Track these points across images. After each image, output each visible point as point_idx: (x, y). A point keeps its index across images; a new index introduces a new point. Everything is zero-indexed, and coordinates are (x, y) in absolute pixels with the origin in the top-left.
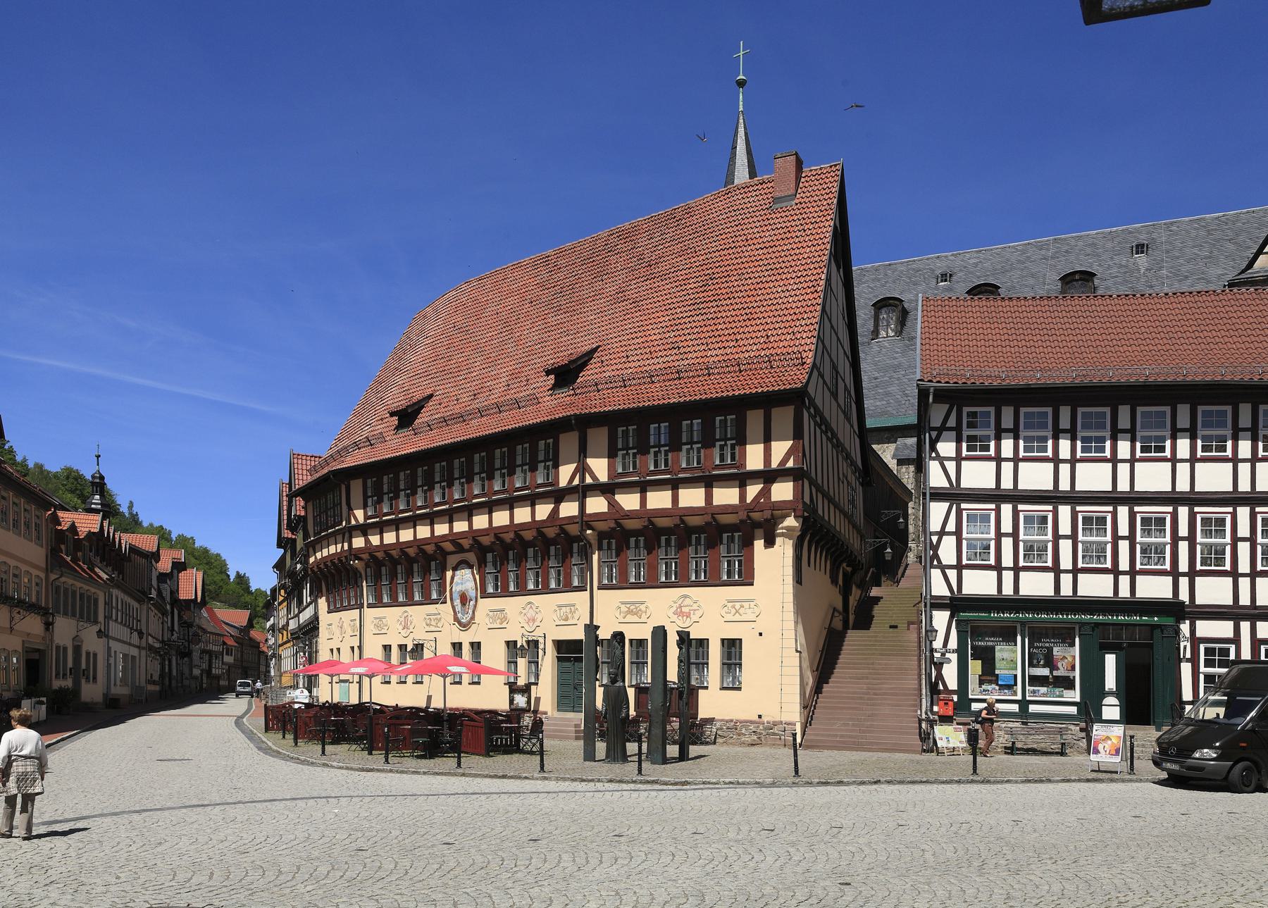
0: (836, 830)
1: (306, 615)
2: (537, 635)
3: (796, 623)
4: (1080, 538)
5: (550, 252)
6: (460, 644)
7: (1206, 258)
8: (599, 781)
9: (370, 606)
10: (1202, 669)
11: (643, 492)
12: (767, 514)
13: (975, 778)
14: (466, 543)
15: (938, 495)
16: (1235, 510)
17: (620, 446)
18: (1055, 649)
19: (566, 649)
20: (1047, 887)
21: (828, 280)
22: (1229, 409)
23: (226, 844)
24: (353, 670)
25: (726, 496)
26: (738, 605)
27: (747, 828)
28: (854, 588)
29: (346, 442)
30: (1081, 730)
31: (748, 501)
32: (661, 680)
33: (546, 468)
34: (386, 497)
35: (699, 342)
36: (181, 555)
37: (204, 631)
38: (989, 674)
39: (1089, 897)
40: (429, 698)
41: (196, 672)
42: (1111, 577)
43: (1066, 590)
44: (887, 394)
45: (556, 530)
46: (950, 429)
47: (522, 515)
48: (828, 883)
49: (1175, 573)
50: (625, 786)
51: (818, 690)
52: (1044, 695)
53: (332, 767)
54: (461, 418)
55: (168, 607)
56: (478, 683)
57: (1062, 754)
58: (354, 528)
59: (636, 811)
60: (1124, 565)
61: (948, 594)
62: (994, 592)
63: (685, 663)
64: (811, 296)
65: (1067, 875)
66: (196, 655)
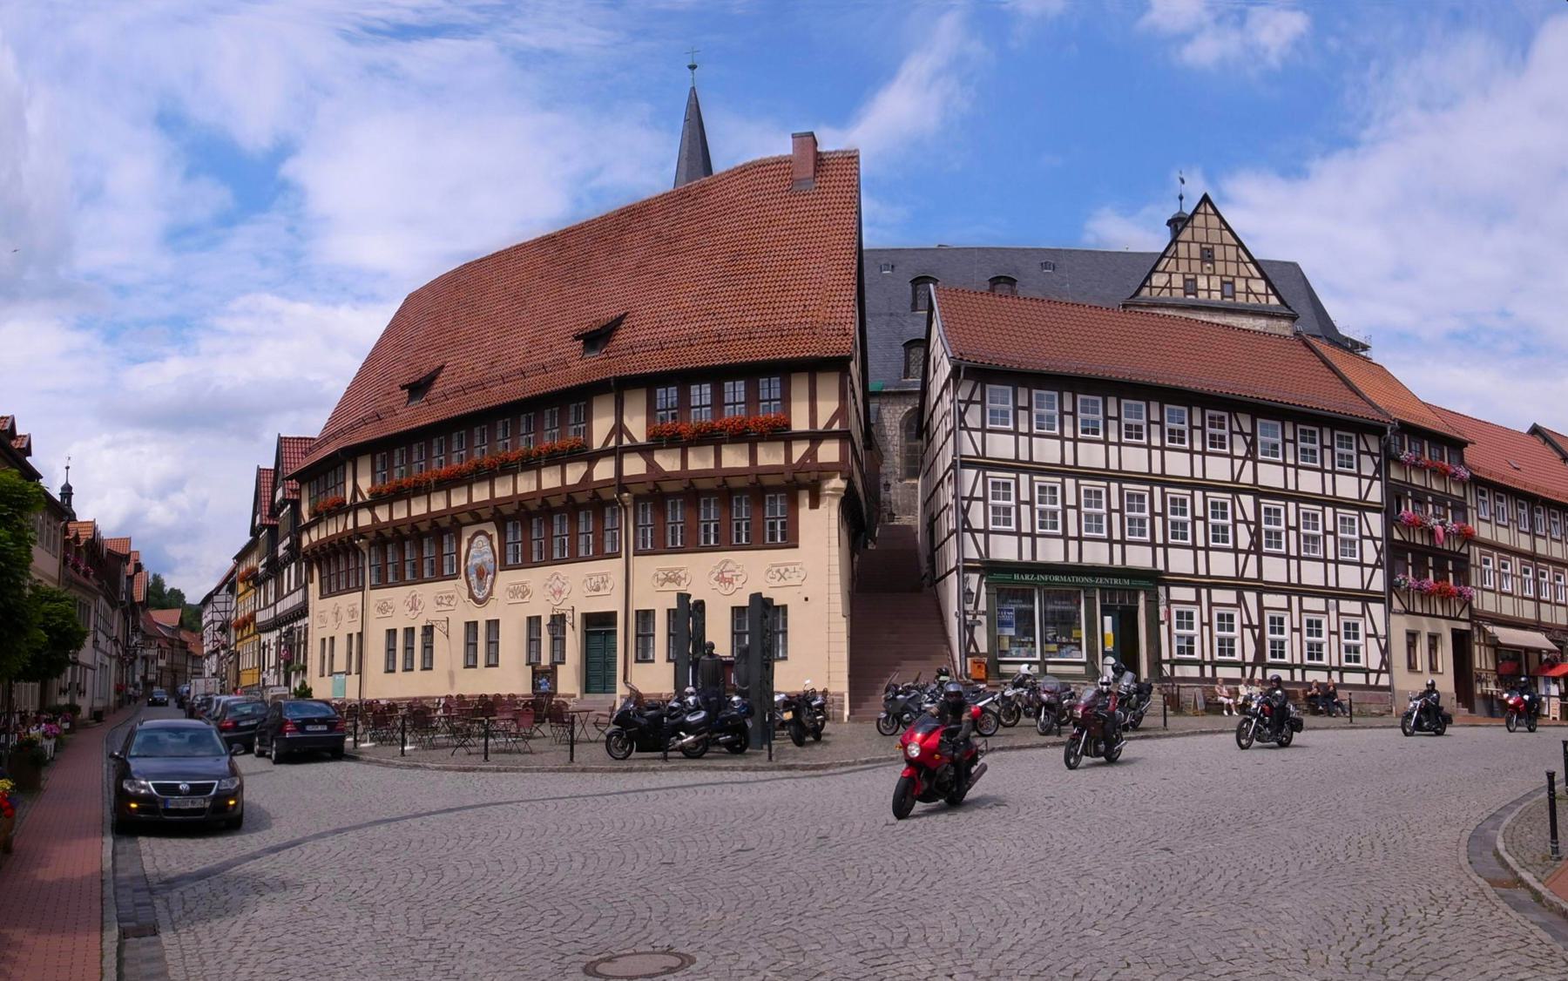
2: (564, 608)
9: (373, 587)
12: (814, 476)
45: (590, 494)
54: (481, 385)
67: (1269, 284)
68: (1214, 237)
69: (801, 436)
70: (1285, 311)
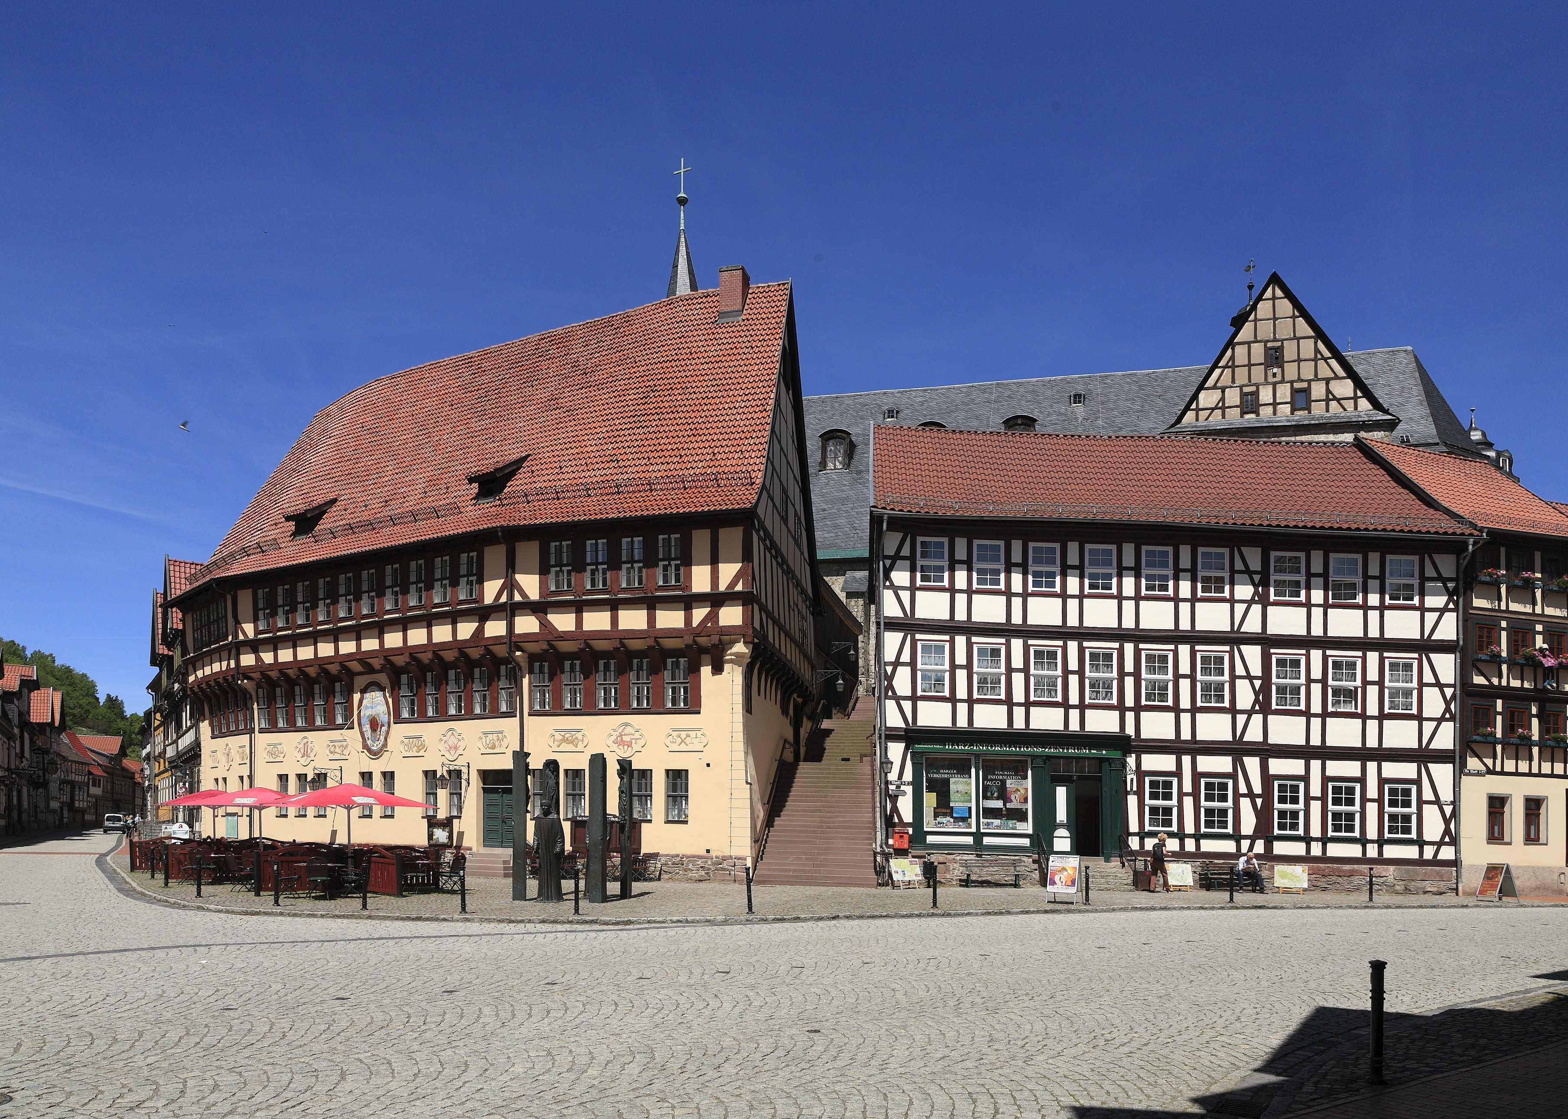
0: (797, 971)
1: (186, 741)
2: (460, 764)
3: (746, 753)
4: (1032, 671)
5: (471, 354)
6: (370, 774)
7: (1138, 411)
8: (530, 921)
9: (261, 731)
10: (1148, 801)
11: (579, 612)
12: (715, 639)
13: (935, 911)
14: (376, 663)
15: (892, 625)
16: (1176, 648)
17: (553, 562)
18: (1008, 782)
19: (492, 780)
20: (1029, 1027)
21: (777, 400)
22: (1170, 549)
23: (49, 1005)
24: (238, 801)
25: (670, 619)
26: (683, 735)
27: (700, 970)
28: (805, 720)
29: (233, 548)
30: (1034, 862)
31: (695, 624)
32: (600, 812)
33: (470, 583)
34: (280, 610)
35: (639, 455)
36: (33, 673)
37: (65, 759)
38: (944, 807)
39: (1074, 1035)
40: (334, 833)
41: (55, 805)
42: (1062, 710)
43: (1019, 723)
44: (836, 526)
45: (481, 651)
46: (904, 558)
47: (442, 633)
48: (794, 1031)
49: (1121, 708)
50: (559, 927)
51: (769, 823)
52: (998, 827)
53: (209, 910)
54: (370, 526)
55: (16, 731)
56: (392, 817)
57: (1016, 885)
58: (234, 642)
59: (573, 955)
60: (1074, 699)
61: (904, 726)
62: (948, 724)
63: (626, 795)
64: (760, 415)
65: (1047, 1012)
66: (54, 787)
67: (1359, 384)
68: (1285, 329)
69: (701, 598)
70: (1381, 416)
